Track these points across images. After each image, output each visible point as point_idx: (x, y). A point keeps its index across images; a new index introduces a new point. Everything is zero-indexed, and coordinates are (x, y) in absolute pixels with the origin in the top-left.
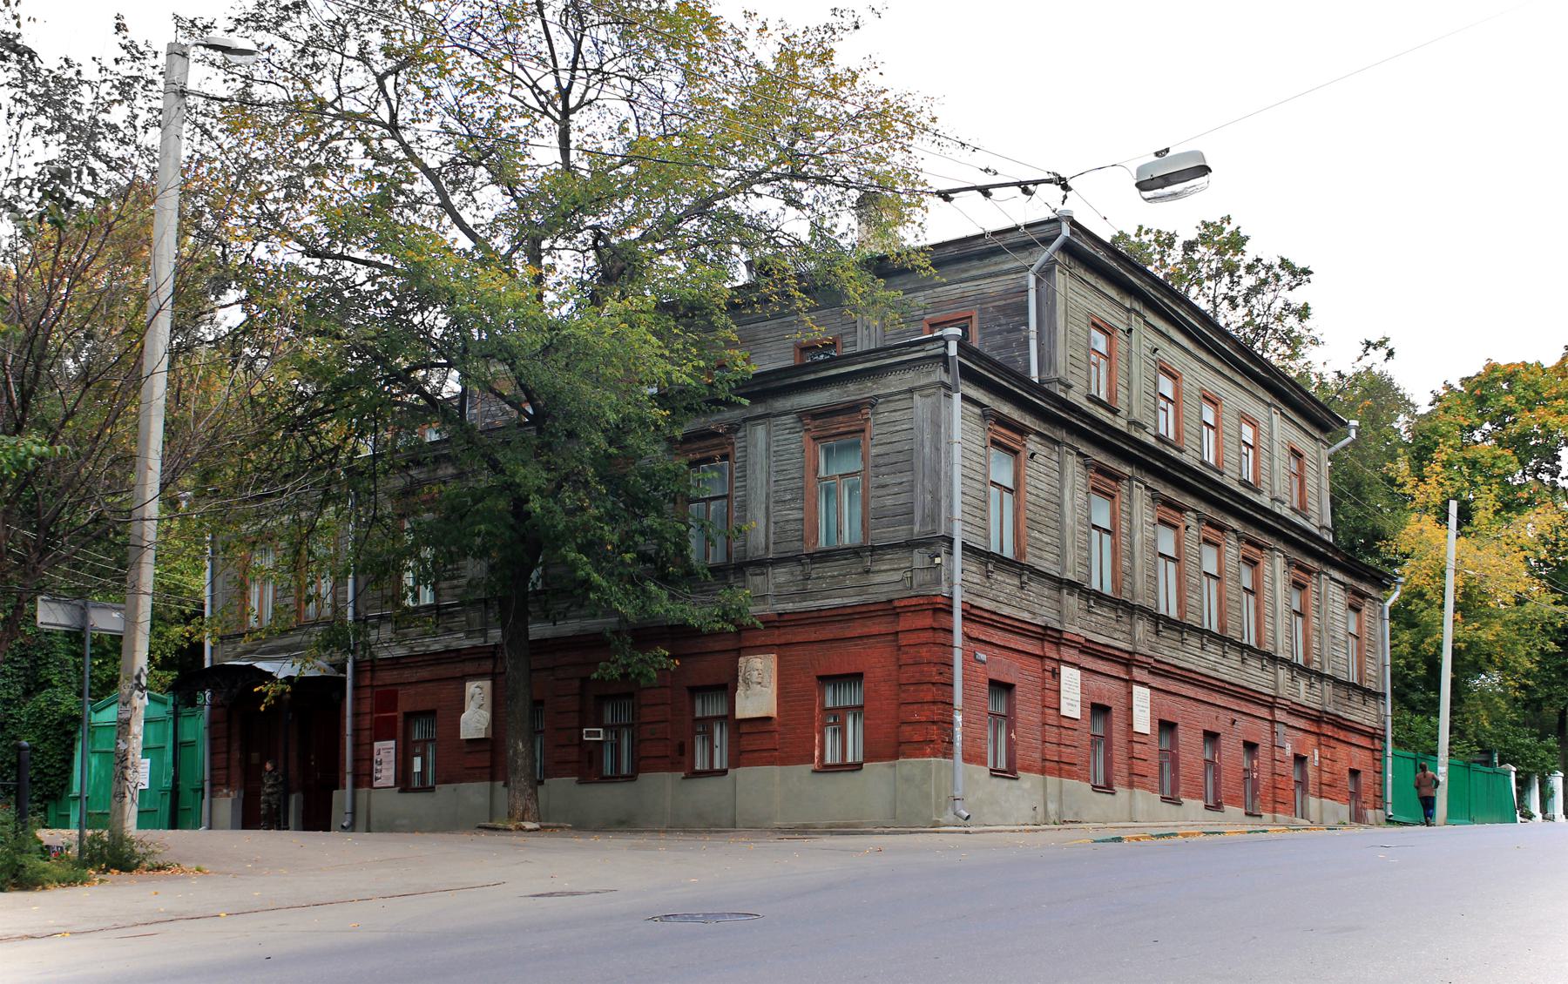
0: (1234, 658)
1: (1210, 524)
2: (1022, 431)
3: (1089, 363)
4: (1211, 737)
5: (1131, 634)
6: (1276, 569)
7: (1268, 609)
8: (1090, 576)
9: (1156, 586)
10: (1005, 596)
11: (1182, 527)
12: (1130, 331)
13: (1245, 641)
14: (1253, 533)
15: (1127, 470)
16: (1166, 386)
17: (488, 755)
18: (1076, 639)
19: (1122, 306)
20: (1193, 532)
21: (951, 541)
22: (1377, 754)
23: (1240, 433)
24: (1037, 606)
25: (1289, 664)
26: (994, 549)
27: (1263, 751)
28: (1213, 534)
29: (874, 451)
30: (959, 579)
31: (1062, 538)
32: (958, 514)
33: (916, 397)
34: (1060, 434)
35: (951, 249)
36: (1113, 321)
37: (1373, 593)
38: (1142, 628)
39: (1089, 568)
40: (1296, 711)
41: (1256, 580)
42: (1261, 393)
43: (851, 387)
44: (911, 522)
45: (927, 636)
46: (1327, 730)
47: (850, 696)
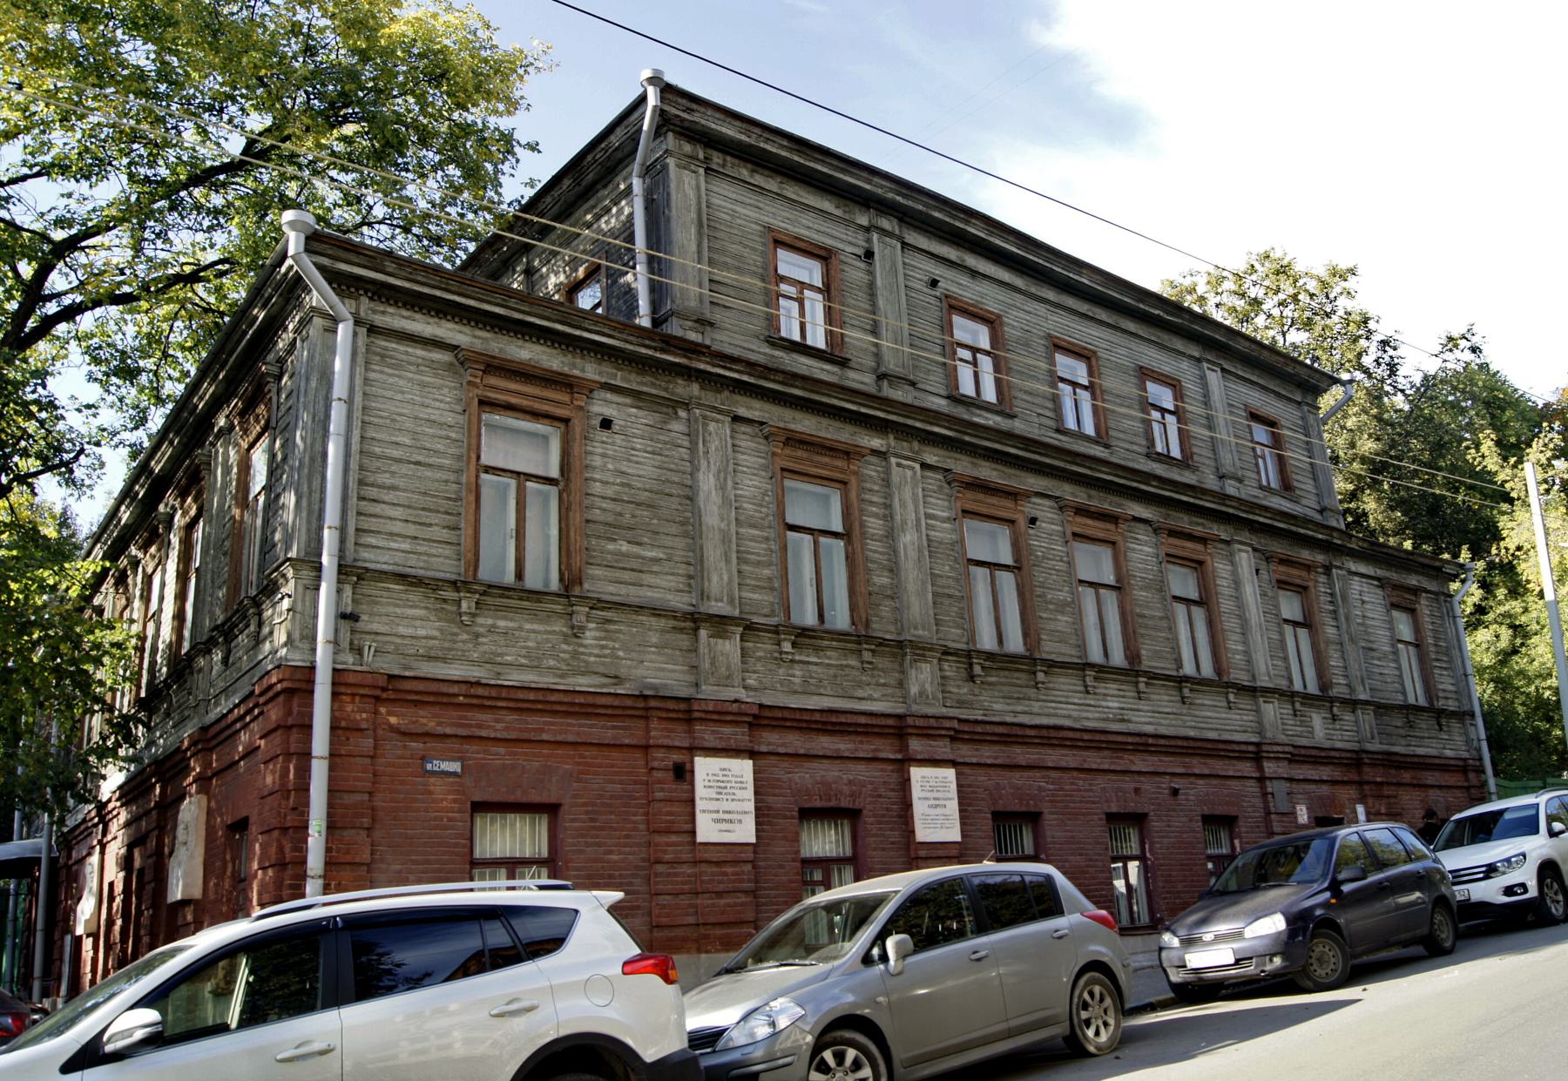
0: (1164, 699)
3: (1256, 457)
7: (1230, 624)
12: (869, 254)
35: (567, 182)
36: (829, 242)
37: (1432, 586)
41: (1205, 585)
42: (1179, 344)
46: (1370, 774)
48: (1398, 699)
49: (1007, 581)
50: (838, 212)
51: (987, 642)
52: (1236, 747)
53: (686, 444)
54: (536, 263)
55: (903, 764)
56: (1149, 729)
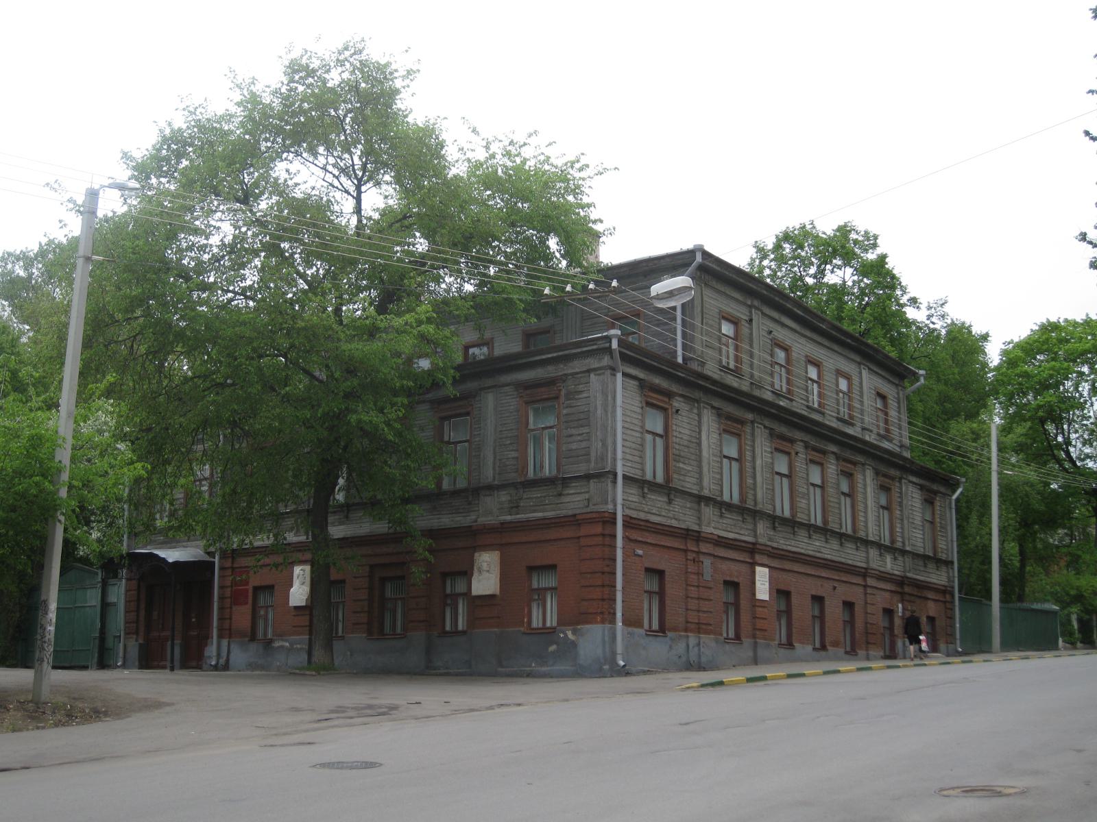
0: (834, 544)
1: (815, 449)
2: (669, 395)
4: (818, 600)
5: (755, 531)
6: (867, 481)
7: (860, 507)
8: (722, 491)
9: (773, 496)
10: (657, 510)
11: (793, 454)
12: (751, 320)
13: (843, 530)
14: (848, 454)
15: (750, 416)
16: (781, 355)
17: (307, 618)
18: (710, 536)
19: (745, 304)
20: (802, 456)
21: (615, 475)
22: (948, 606)
23: (837, 385)
24: (681, 515)
25: (879, 545)
26: (649, 477)
28: (816, 456)
29: (565, 412)
30: (621, 500)
31: (700, 467)
32: (619, 455)
33: (592, 375)
34: (697, 394)
36: (739, 315)
37: (942, 489)
38: (762, 528)
39: (722, 486)
40: (883, 577)
41: (852, 487)
42: (853, 356)
43: (550, 368)
44: (589, 461)
45: (599, 540)
47: (548, 581)
48: (768, 509)
49: (660, 442)
50: (741, 298)
52: (857, 569)
53: (697, 418)
55: (753, 565)
56: (829, 557)
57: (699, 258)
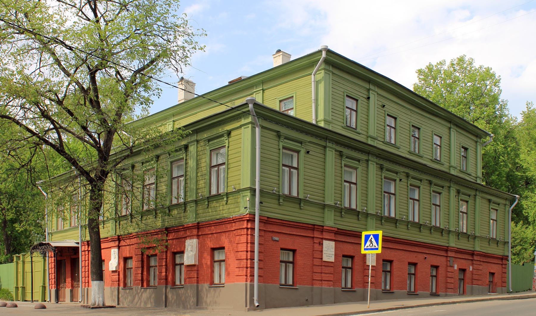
12: (369, 98)
27: (441, 270)
51: (411, 219)
54: (504, 179)
57: (324, 54)
